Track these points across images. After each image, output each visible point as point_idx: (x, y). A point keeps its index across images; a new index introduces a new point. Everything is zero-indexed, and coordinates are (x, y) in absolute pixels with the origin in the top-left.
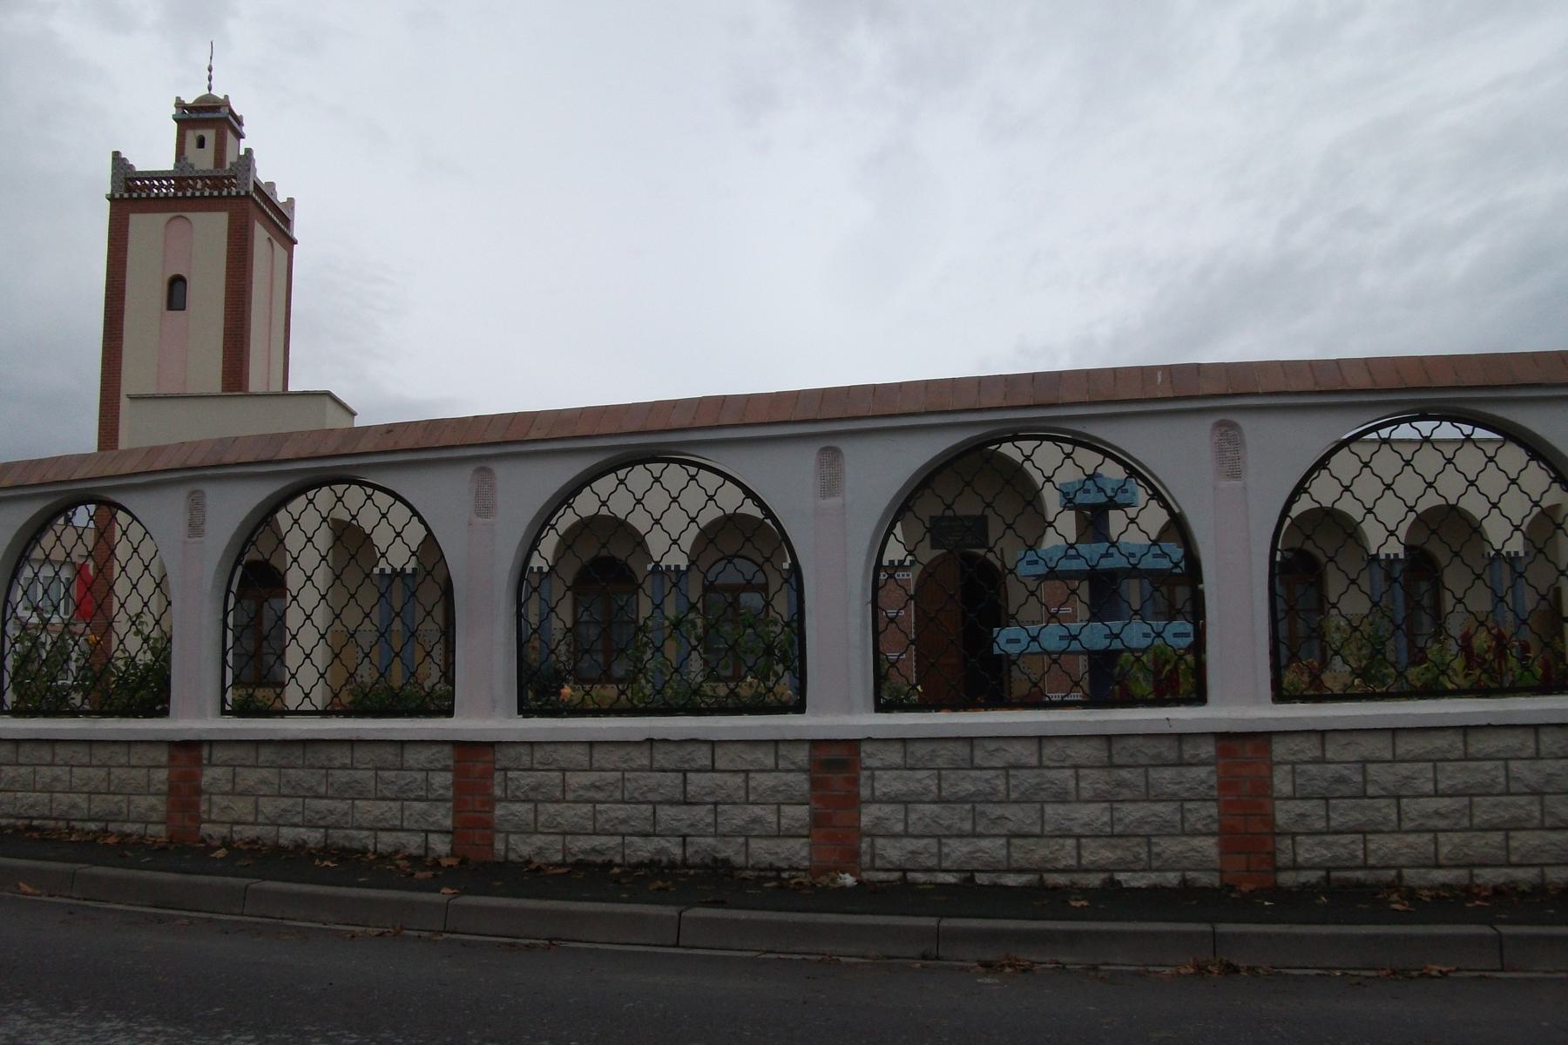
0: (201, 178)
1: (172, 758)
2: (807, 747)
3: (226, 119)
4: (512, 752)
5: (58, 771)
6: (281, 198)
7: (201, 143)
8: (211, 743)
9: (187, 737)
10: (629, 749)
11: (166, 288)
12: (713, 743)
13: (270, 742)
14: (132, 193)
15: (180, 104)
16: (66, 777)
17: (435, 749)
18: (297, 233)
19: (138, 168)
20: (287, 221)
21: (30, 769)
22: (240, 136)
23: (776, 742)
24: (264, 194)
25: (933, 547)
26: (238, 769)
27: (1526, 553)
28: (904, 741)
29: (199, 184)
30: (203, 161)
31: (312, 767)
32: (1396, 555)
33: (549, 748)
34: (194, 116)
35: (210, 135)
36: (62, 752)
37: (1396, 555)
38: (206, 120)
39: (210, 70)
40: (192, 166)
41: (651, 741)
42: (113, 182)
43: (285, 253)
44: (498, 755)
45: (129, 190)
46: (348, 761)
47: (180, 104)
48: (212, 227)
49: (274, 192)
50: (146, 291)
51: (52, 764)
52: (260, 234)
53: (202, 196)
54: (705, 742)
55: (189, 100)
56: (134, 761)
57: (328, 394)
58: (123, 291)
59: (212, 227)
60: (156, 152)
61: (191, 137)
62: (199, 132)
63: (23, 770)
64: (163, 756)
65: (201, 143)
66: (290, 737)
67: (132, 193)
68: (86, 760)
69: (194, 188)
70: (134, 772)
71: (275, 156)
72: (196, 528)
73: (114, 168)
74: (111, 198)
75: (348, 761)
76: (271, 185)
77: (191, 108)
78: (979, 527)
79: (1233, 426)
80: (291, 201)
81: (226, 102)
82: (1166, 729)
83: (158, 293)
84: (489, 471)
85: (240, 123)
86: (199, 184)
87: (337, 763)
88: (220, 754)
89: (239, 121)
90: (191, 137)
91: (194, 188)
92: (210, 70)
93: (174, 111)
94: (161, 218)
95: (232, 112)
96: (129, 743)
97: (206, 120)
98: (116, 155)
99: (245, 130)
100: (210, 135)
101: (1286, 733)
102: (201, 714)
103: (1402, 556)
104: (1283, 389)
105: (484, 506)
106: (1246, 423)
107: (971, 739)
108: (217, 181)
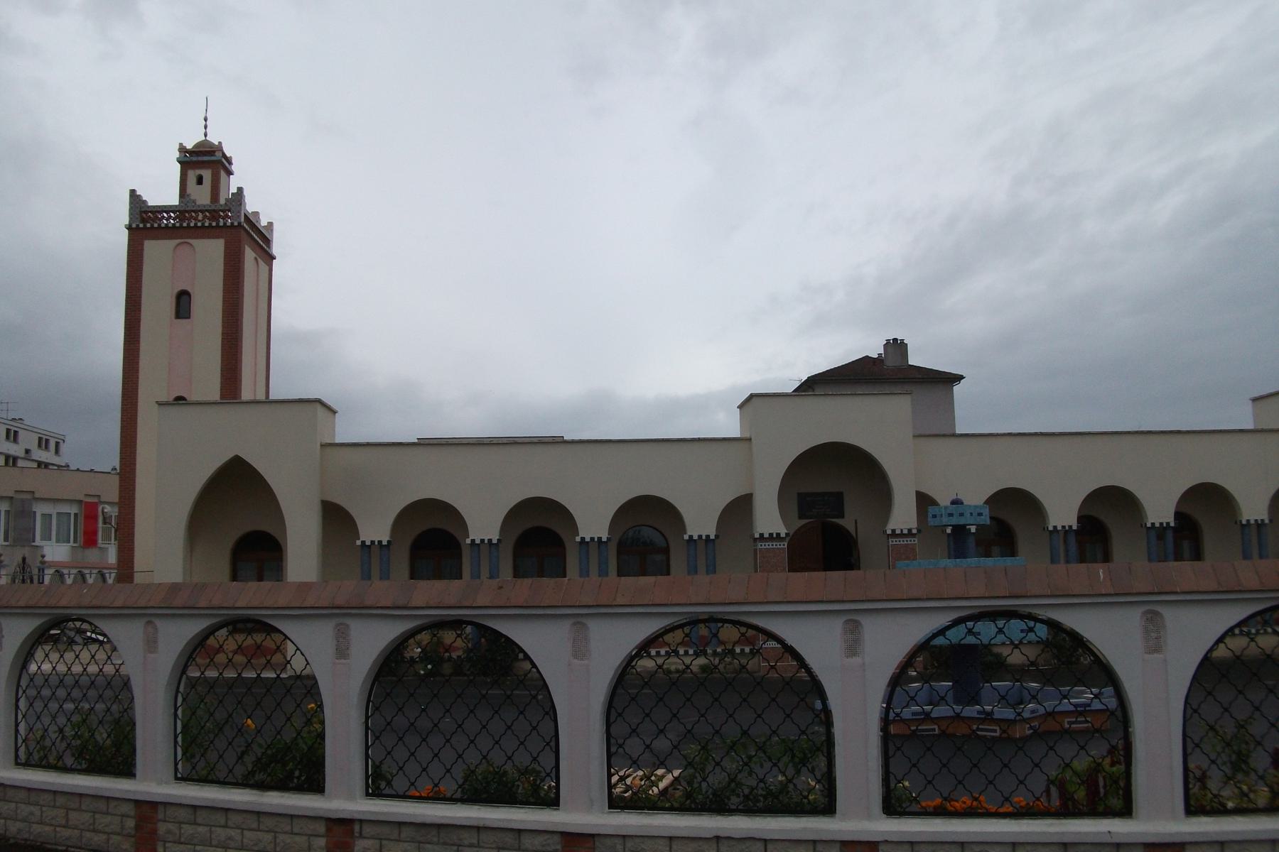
0: (202, 211)
1: (329, 830)
2: (838, 845)
3: (220, 162)
4: (608, 842)
5: (232, 833)
6: (264, 222)
7: (200, 181)
8: (361, 821)
9: (342, 816)
10: (701, 843)
11: (174, 300)
12: (765, 840)
13: (411, 823)
14: (145, 222)
15: (182, 149)
16: (238, 838)
17: (547, 837)
18: (276, 249)
19: (150, 203)
20: (268, 241)
21: (207, 829)
22: (230, 173)
23: (814, 842)
24: (251, 221)
25: (800, 517)
26: (384, 842)
27: (1271, 521)
28: (911, 843)
29: (200, 217)
30: (202, 196)
31: (445, 844)
32: (1168, 524)
33: (637, 840)
34: (194, 159)
35: (207, 174)
36: (235, 819)
37: (1168, 524)
38: (204, 161)
39: (206, 120)
40: (194, 202)
41: (718, 838)
42: (131, 214)
43: (267, 268)
44: (597, 844)
45: (144, 221)
46: (475, 841)
47: (182, 149)
48: (212, 251)
49: (258, 220)
50: (158, 304)
51: (226, 826)
52: (249, 254)
53: (203, 226)
54: (760, 840)
55: (189, 145)
56: (296, 830)
57: (319, 401)
58: (140, 305)
59: (212, 251)
60: (164, 191)
61: (192, 175)
62: (199, 172)
63: (200, 829)
64: (321, 828)
65: (200, 181)
66: (428, 821)
67: (145, 222)
68: (255, 825)
69: (196, 219)
70: (297, 838)
71: (258, 185)
72: (342, 652)
73: (131, 203)
74: (129, 228)
75: (475, 841)
76: (256, 214)
77: (191, 152)
78: (836, 502)
79: (1157, 613)
80: (270, 224)
81: (219, 148)
82: (1108, 839)
83: (169, 305)
84: (584, 625)
85: (230, 163)
86: (200, 217)
87: (466, 842)
88: (367, 830)
89: (229, 161)
90: (192, 175)
91: (196, 219)
92: (206, 120)
93: (177, 154)
94: (172, 243)
95: (224, 155)
96: (292, 816)
97: (204, 161)
98: (133, 192)
99: (234, 168)
100: (207, 174)
101: (1196, 843)
102: (351, 798)
103: (1172, 524)
104: (1195, 589)
105: (580, 650)
106: (1168, 614)
107: (962, 843)
108: (214, 214)
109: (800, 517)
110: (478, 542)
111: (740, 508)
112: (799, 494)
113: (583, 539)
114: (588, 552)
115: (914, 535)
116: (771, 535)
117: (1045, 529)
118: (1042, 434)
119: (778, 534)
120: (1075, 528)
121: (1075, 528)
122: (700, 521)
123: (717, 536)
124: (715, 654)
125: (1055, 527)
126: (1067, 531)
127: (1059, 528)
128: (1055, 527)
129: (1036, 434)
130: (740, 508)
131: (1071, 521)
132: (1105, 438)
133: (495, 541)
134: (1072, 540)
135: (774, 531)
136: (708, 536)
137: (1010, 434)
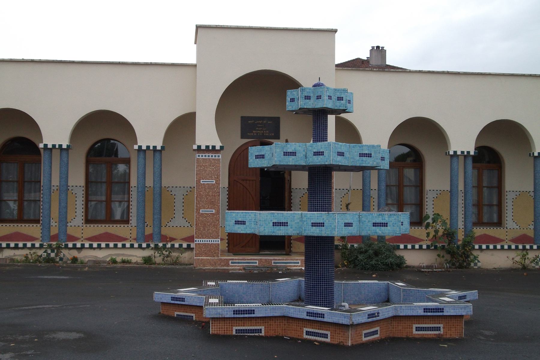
25: (243, 137)
37: (468, 152)
109: (243, 137)
110: (144, 148)
111: (184, 124)
112: (242, 117)
113: (140, 147)
114: (145, 159)
115: (218, 151)
116: (207, 147)
117: (447, 154)
118: (448, 73)
119: (214, 147)
120: (472, 153)
121: (472, 153)
122: (149, 134)
123: (163, 148)
124: (156, 247)
125: (455, 152)
126: (466, 156)
127: (459, 153)
128: (455, 152)
129: (443, 73)
130: (184, 124)
131: (470, 148)
132: (503, 79)
133: (159, 148)
134: (470, 162)
135: (211, 144)
136: (155, 147)
137: (420, 72)
